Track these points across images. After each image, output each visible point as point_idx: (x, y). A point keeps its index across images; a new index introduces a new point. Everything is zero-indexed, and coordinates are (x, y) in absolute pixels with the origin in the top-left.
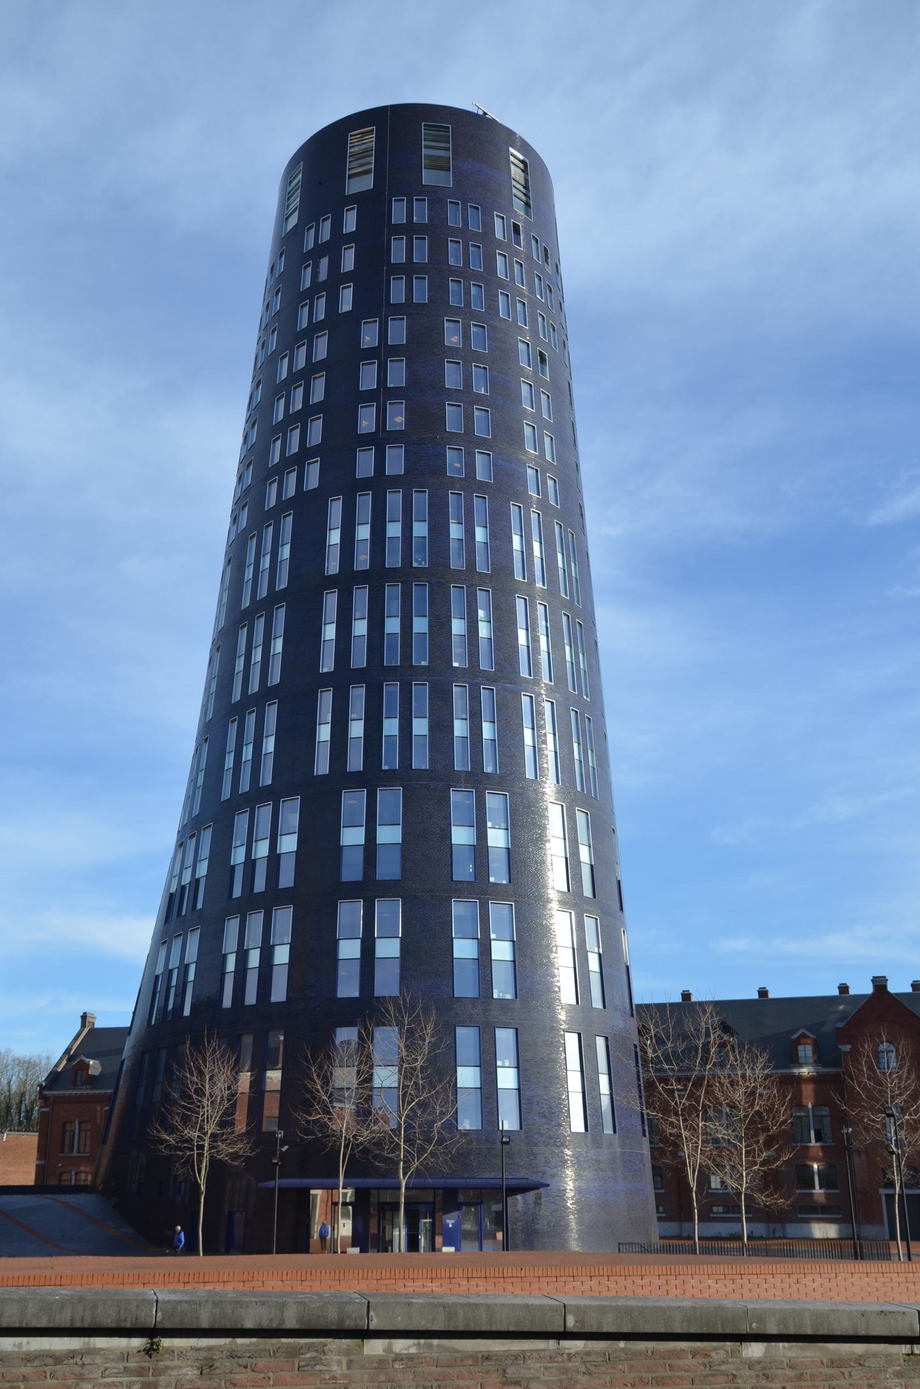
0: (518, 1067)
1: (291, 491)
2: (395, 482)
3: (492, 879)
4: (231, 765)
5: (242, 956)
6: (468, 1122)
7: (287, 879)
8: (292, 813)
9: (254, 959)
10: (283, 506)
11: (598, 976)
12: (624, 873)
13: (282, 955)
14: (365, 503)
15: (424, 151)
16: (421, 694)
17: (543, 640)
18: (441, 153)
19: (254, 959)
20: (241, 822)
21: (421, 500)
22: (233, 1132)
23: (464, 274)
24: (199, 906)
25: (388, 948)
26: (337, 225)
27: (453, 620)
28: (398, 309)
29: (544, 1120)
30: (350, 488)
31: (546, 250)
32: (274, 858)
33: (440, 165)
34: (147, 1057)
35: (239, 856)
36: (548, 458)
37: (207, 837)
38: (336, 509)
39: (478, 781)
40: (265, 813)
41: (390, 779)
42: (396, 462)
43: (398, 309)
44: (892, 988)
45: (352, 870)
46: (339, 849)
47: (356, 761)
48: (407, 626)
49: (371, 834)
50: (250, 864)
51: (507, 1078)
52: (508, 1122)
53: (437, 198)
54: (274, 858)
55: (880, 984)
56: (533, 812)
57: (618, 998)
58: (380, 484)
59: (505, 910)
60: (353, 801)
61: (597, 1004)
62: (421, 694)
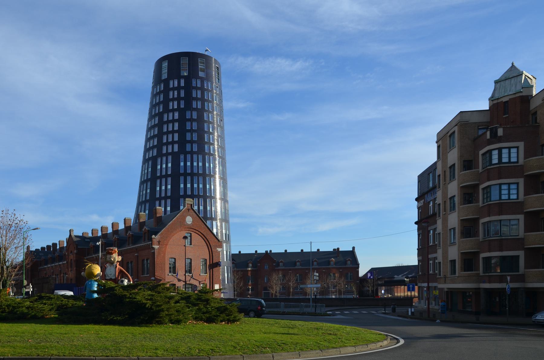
2: (195, 153)
10: (167, 154)
16: (201, 179)
21: (200, 157)
26: (179, 83)
30: (186, 153)
33: (203, 71)
38: (182, 157)
42: (195, 148)
58: (192, 153)
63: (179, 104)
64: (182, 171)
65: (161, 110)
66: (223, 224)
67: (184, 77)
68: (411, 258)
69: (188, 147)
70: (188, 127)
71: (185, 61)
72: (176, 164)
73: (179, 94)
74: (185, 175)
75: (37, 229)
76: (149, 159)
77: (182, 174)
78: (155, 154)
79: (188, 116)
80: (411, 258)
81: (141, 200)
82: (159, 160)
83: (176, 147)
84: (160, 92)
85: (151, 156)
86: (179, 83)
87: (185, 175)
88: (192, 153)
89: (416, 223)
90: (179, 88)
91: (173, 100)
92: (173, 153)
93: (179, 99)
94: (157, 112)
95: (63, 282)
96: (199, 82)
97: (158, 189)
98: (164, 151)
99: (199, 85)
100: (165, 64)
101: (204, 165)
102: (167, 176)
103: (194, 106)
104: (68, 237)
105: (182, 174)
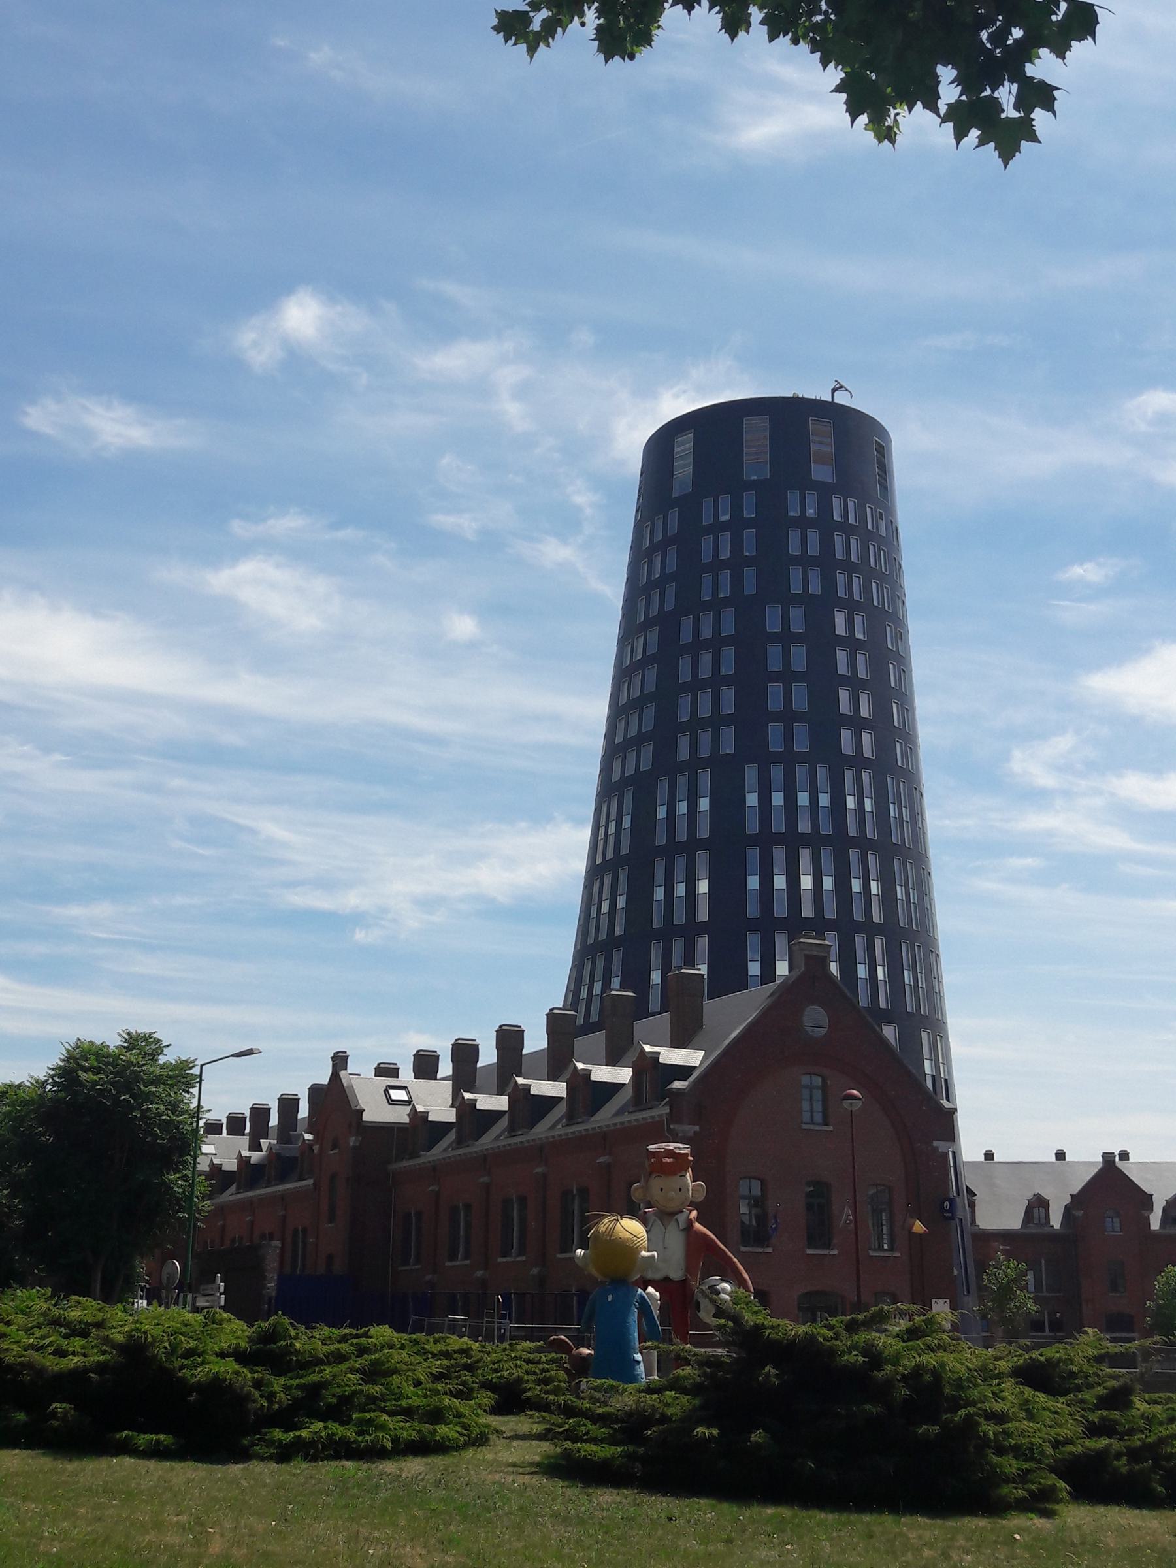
2: (803, 757)
6: (863, 1001)
10: (693, 766)
14: (777, 772)
21: (822, 773)
22: (605, 1403)
23: (850, 568)
28: (796, 600)
30: (765, 761)
38: (752, 774)
42: (802, 741)
43: (796, 600)
53: (825, 492)
58: (789, 759)
63: (737, 581)
64: (753, 910)
65: (670, 605)
70: (775, 703)
71: (758, 431)
72: (728, 803)
73: (737, 545)
75: (250, 1052)
76: (625, 782)
77: (753, 840)
78: (646, 765)
79: (773, 624)
81: (591, 940)
82: (663, 787)
83: (728, 736)
84: (666, 542)
85: (630, 770)
86: (737, 508)
88: (789, 759)
89: (1072, 1196)
91: (717, 528)
92: (716, 762)
93: (737, 564)
94: (654, 611)
95: (377, 1245)
96: (811, 499)
97: (659, 894)
98: (683, 754)
99: (813, 550)
100: (685, 445)
103: (796, 588)
104: (324, 1079)
105: (754, 925)
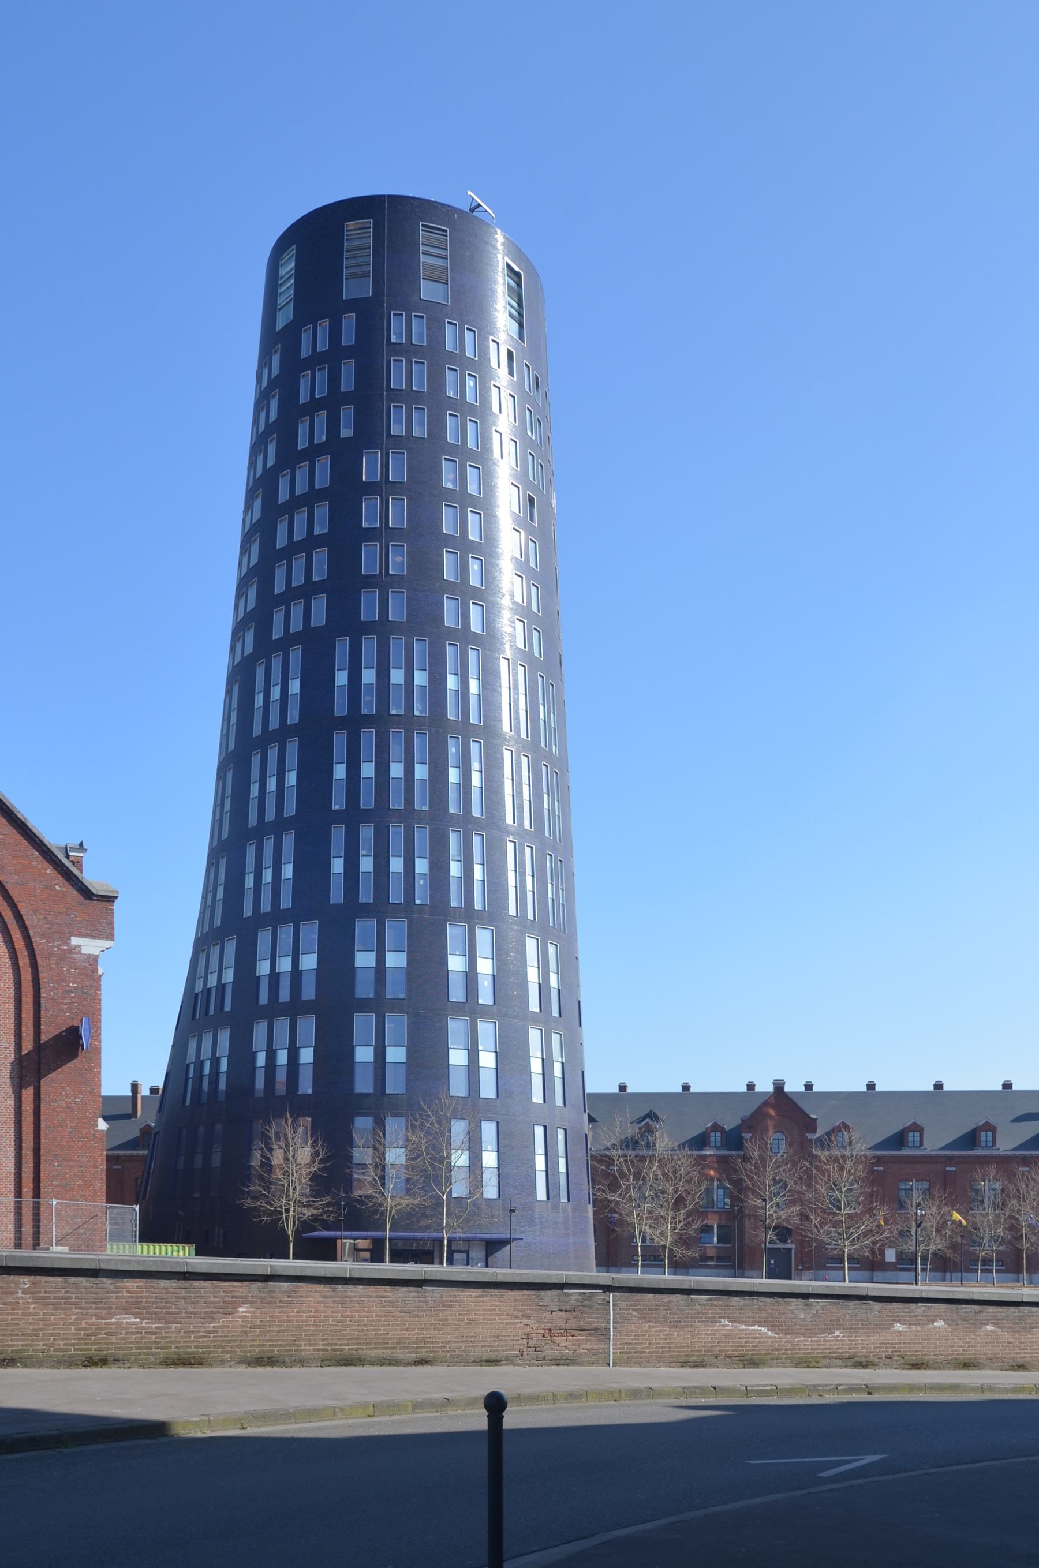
0: (498, 1151)
1: (296, 625)
3: (480, 1001)
4: (252, 885)
5: (271, 1056)
7: (309, 992)
8: (311, 931)
9: (282, 1057)
10: (289, 640)
11: (561, 1080)
12: (585, 995)
13: (307, 1056)
15: (423, 258)
16: (422, 837)
17: (529, 879)
18: (440, 262)
19: (282, 1057)
20: (264, 938)
24: (227, 1008)
25: (396, 1055)
26: (335, 333)
27: (450, 769)
29: (516, 1191)
31: (537, 378)
32: (296, 973)
33: (439, 279)
34: (185, 1132)
35: (263, 968)
36: (536, 654)
37: (231, 948)
39: (469, 917)
40: (285, 933)
41: (396, 911)
44: (787, 1089)
45: (364, 989)
46: (352, 969)
47: (366, 895)
48: (409, 771)
49: (381, 959)
50: (274, 977)
51: (489, 1159)
52: (490, 1191)
54: (296, 973)
55: (779, 1086)
56: (495, 694)
57: (575, 1097)
58: (383, 629)
59: (491, 1026)
60: (363, 928)
61: (559, 1102)
62: (422, 837)
66: (555, 1038)
67: (354, 305)
68: (388, 1091)
69: (368, 608)
71: (358, 233)
73: (334, 380)
74: (355, 722)
77: (341, 723)
80: (388, 1091)
87: (355, 722)
88: (383, 629)
90: (334, 355)
101: (437, 681)
102: (280, 825)
